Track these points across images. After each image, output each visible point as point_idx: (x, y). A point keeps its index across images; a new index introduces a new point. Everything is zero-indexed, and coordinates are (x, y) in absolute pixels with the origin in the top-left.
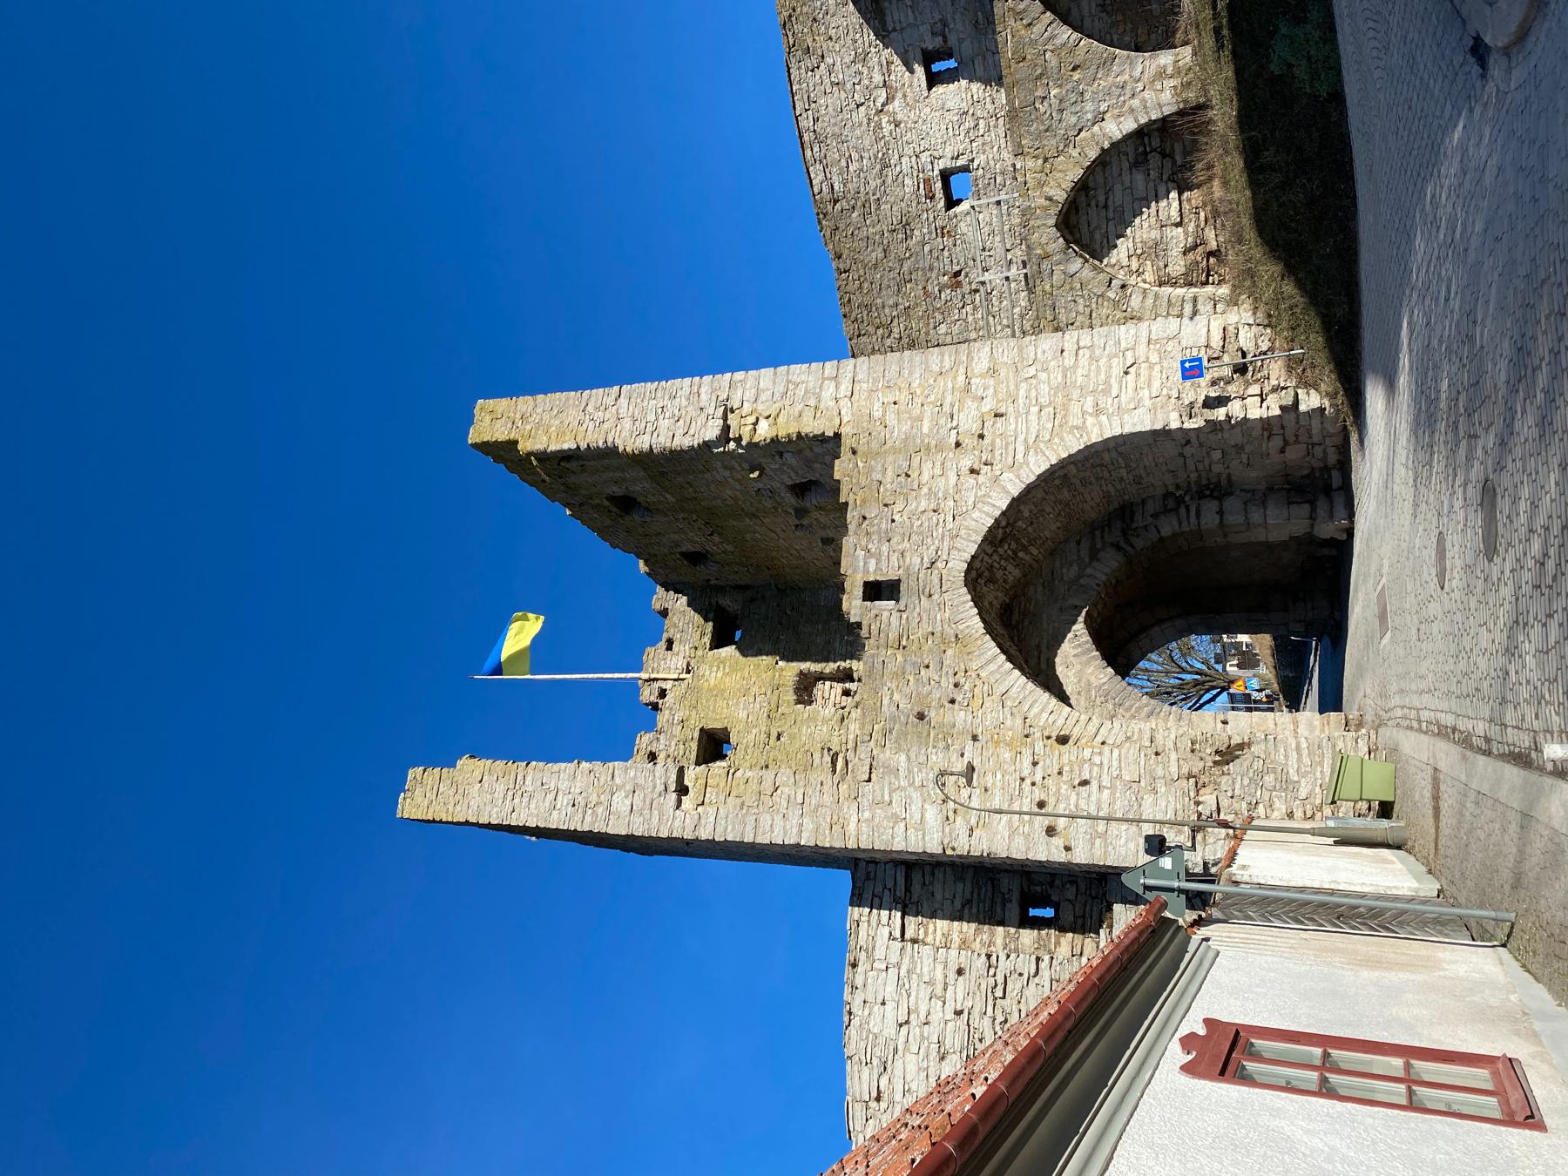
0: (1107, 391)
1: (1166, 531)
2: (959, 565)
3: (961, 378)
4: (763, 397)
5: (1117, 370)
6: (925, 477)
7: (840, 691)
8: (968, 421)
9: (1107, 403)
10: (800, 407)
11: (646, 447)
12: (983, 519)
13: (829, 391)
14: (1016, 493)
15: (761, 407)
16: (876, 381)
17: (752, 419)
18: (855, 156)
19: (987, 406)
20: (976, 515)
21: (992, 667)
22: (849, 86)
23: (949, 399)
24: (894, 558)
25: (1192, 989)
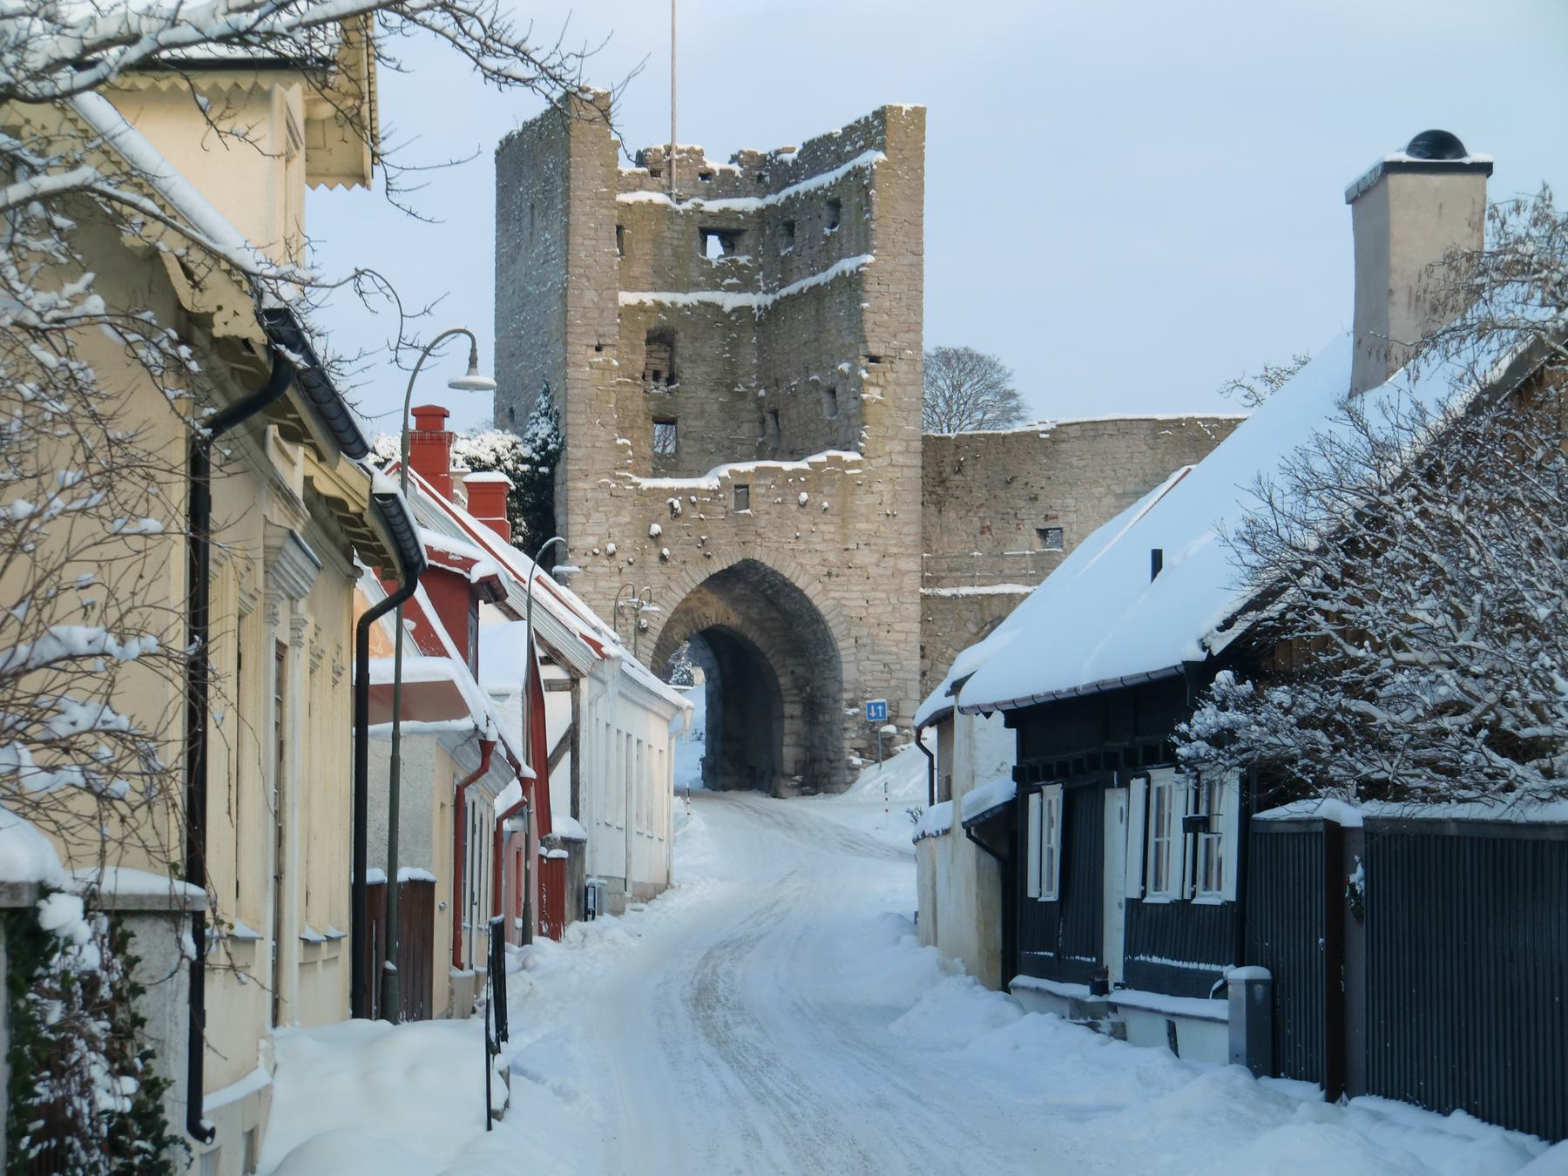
0: (873, 652)
1: (782, 680)
2: (761, 555)
3: (895, 550)
4: (898, 390)
5: (888, 659)
6: (822, 527)
7: (659, 368)
8: (864, 557)
9: (863, 654)
10: (887, 423)
11: (868, 287)
12: (790, 571)
13: (898, 446)
14: (806, 592)
15: (890, 389)
16: (902, 484)
17: (882, 381)
18: (1083, 463)
19: (872, 571)
20: (793, 565)
21: (688, 579)
22: (1129, 466)
23: (879, 541)
24: (765, 507)
25: (1558, 1047)
